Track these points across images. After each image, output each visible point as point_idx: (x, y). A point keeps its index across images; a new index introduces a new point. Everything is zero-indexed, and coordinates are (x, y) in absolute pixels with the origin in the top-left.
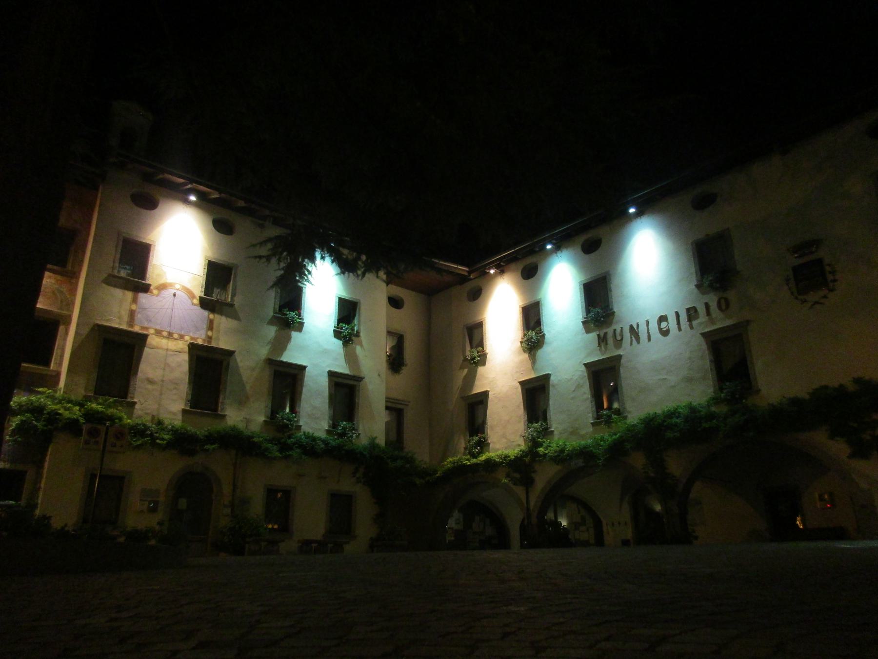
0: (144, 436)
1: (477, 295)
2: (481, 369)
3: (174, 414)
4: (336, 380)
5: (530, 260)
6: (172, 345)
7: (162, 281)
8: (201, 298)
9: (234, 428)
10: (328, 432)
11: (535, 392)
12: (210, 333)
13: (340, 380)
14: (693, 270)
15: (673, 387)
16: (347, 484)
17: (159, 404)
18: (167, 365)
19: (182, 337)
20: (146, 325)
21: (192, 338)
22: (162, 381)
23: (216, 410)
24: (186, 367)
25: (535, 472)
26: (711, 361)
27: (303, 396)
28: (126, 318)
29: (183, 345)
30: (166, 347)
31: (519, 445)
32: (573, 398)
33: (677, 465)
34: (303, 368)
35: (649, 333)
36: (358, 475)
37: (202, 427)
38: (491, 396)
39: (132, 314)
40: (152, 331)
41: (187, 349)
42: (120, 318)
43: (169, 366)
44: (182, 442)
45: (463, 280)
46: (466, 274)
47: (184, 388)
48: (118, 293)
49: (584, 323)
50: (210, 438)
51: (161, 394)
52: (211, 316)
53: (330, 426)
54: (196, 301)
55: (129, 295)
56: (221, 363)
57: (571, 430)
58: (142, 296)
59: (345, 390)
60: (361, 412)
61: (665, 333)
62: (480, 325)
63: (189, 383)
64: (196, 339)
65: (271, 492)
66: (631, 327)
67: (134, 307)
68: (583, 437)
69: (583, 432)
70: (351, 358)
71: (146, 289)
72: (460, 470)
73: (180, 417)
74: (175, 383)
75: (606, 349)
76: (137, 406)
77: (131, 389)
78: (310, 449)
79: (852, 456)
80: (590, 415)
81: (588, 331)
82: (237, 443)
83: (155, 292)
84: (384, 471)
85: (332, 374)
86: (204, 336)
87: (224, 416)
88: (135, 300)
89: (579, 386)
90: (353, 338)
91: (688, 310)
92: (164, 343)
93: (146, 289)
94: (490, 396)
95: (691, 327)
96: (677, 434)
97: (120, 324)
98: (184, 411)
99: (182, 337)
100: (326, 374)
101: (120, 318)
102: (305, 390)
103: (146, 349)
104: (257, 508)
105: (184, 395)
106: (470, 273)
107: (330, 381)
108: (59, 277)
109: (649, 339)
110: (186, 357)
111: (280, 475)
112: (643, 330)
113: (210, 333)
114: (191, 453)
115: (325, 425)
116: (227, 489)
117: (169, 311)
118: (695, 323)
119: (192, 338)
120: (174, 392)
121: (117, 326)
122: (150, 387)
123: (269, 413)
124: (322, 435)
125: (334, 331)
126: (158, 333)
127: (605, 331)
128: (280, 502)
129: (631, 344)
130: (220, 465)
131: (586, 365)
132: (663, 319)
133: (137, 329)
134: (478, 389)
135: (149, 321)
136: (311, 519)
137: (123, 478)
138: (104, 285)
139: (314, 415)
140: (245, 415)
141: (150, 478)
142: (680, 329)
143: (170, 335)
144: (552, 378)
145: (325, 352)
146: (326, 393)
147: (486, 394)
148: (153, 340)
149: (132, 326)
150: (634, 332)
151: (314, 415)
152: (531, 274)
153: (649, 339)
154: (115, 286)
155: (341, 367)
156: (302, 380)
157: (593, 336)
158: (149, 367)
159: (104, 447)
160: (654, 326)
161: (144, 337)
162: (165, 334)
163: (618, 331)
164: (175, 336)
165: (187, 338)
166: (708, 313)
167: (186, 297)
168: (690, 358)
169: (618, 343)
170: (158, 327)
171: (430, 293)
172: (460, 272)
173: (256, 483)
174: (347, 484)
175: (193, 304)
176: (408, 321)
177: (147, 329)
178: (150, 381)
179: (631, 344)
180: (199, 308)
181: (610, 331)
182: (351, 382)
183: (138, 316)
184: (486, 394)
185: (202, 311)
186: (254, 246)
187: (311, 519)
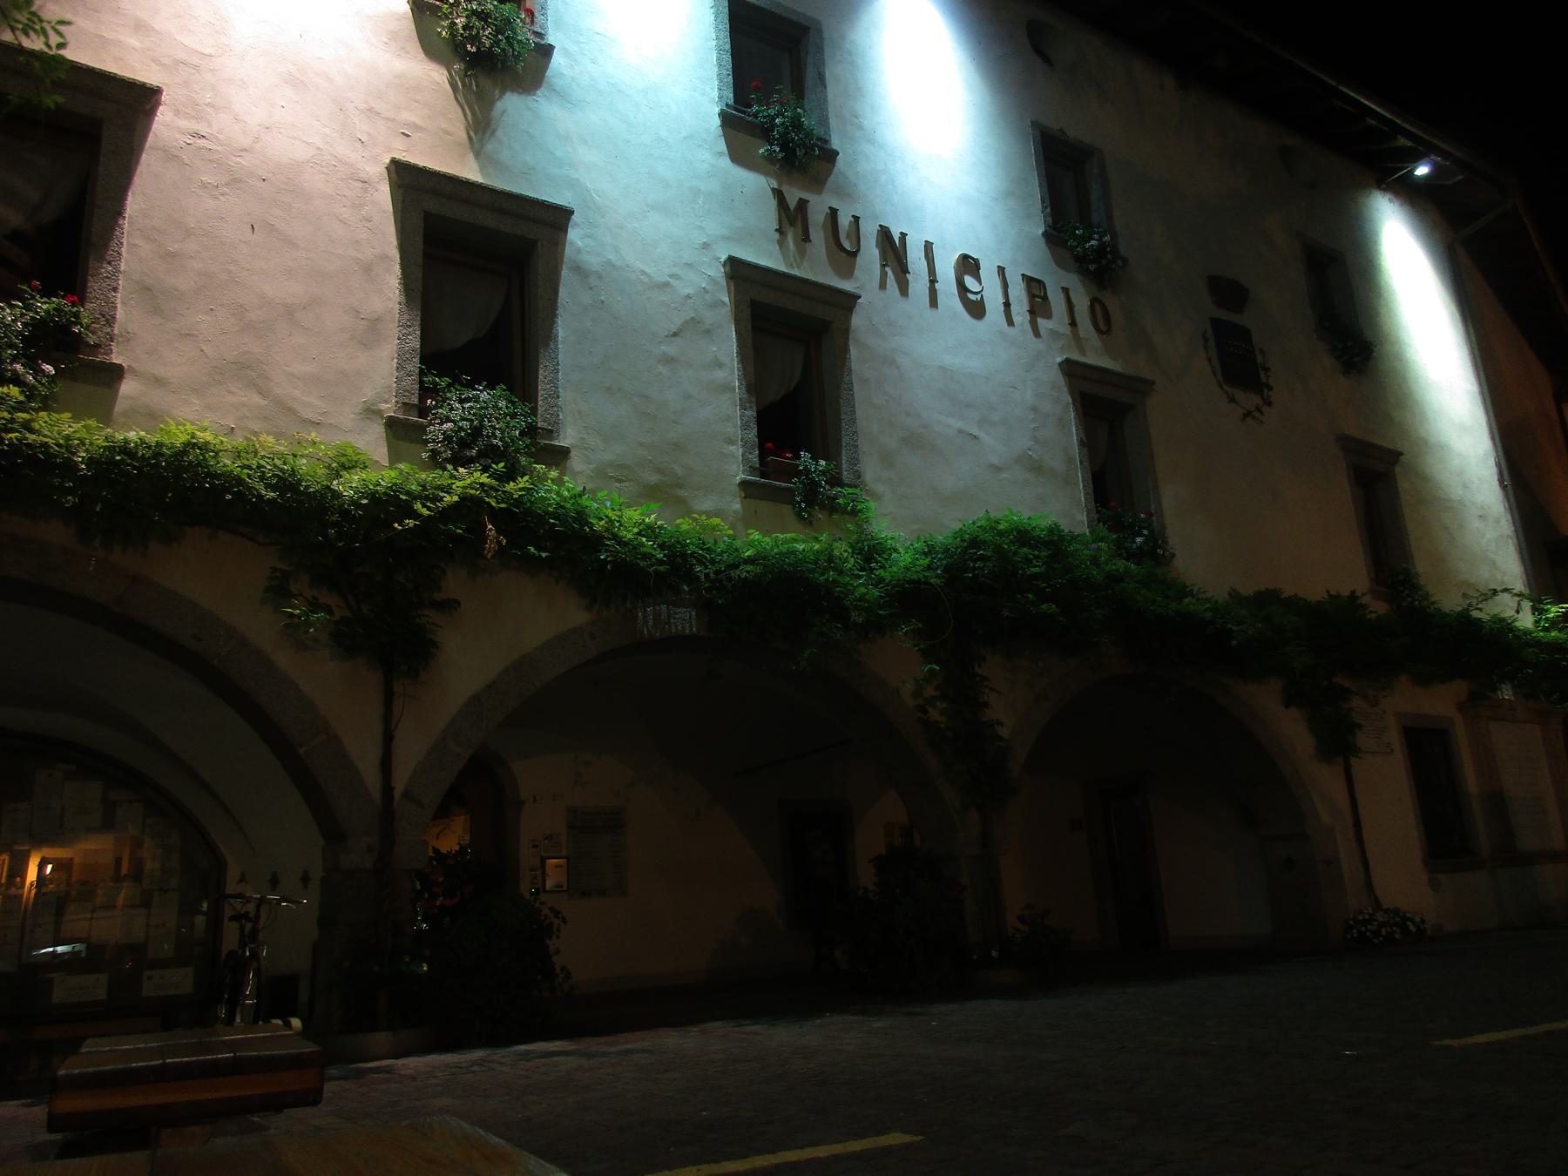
33: (1012, 701)
35: (933, 281)
38: (166, 124)
57: (654, 478)
61: (976, 309)
66: (885, 233)
75: (802, 253)
80: (737, 451)
89: (692, 327)
90: (31, 33)
96: (456, 498)
112: (915, 257)
127: (805, 196)
129: (883, 286)
132: (968, 265)
142: (1010, 322)
150: (893, 250)
153: (934, 303)
160: (946, 268)
163: (844, 221)
179: (883, 286)
186: (196, 67)
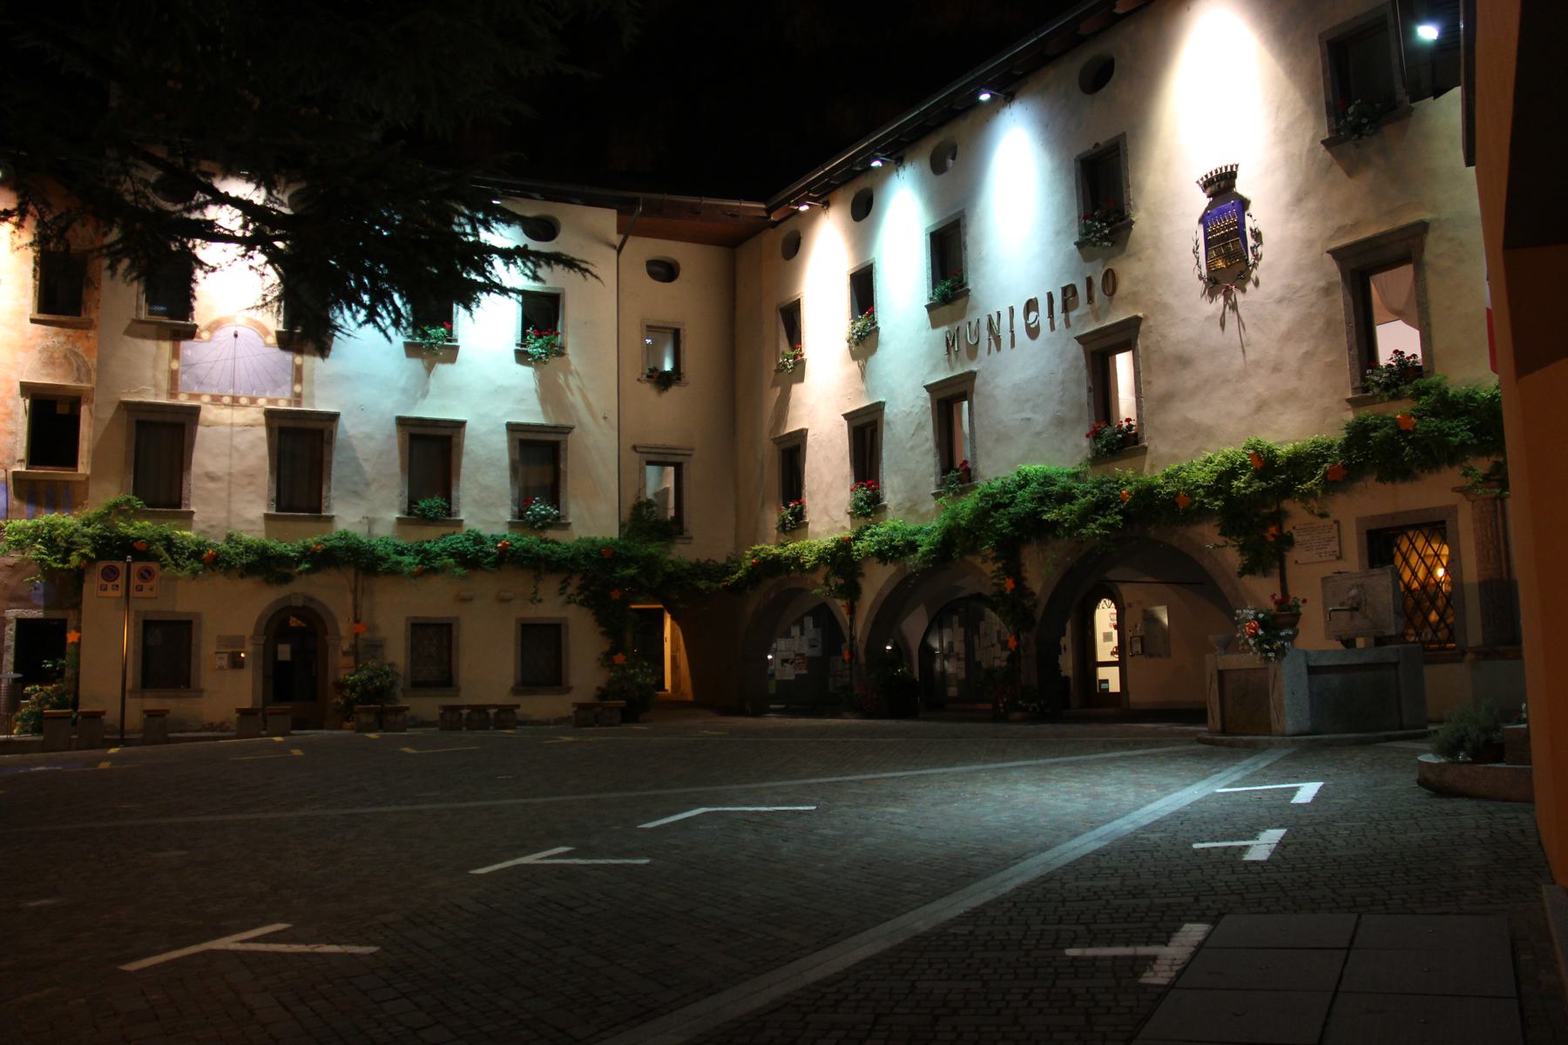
0: (211, 561)
1: (793, 247)
2: (797, 389)
3: (252, 522)
4: (523, 436)
5: (862, 184)
6: (239, 416)
7: (215, 316)
8: (278, 333)
9: (345, 536)
10: (511, 525)
11: (865, 430)
12: (298, 388)
13: (530, 436)
14: (1075, 214)
15: (1039, 434)
16: (551, 605)
17: (229, 511)
18: (232, 447)
19: (253, 401)
20: (196, 390)
21: (270, 401)
22: (230, 474)
23: (319, 510)
24: (263, 449)
25: (862, 575)
26: (1090, 390)
27: (463, 471)
28: (165, 384)
29: (255, 414)
30: (229, 421)
31: (844, 528)
32: (912, 448)
34: (460, 425)
36: (570, 590)
37: (300, 537)
39: (174, 376)
40: (206, 399)
41: (262, 419)
42: (156, 386)
43: (237, 450)
44: (263, 565)
45: (762, 226)
46: (764, 214)
47: (265, 480)
48: (150, 346)
49: (930, 308)
50: (307, 554)
51: (230, 495)
52: (298, 360)
53: (514, 516)
54: (272, 339)
55: (167, 346)
56: (321, 432)
58: (186, 346)
59: (539, 453)
60: (573, 486)
62: (796, 306)
63: (271, 473)
64: (274, 401)
65: (419, 629)
67: (175, 365)
68: (923, 517)
69: (923, 510)
70: (549, 393)
71: (191, 333)
72: (774, 566)
73: (261, 525)
74: (251, 475)
76: (195, 518)
77: (185, 492)
78: (476, 558)
79: (1247, 570)
81: (935, 324)
82: (357, 560)
83: (205, 335)
84: (631, 580)
85: (512, 428)
86: (288, 395)
87: (330, 519)
88: (176, 354)
91: (1065, 290)
92: (225, 415)
93: (191, 333)
94: (810, 439)
95: (1068, 324)
97: (156, 395)
98: (267, 517)
99: (253, 401)
100: (504, 429)
101: (156, 386)
102: (465, 461)
103: (200, 429)
104: (397, 654)
105: (265, 492)
106: (769, 211)
107: (511, 441)
108: (70, 331)
109: (1013, 345)
110: (262, 432)
111: (432, 600)
113: (298, 388)
114: (286, 579)
115: (506, 514)
116: (345, 627)
117: (229, 363)
118: (1073, 314)
119: (270, 401)
120: (252, 488)
121: (152, 400)
122: (211, 485)
123: (406, 506)
124: (500, 530)
125: (517, 352)
126: (216, 400)
128: (435, 641)
130: (330, 593)
131: (928, 388)
133: (183, 400)
134: (792, 427)
135: (201, 383)
136: (488, 668)
137: (190, 622)
138: (128, 338)
139: (485, 502)
140: (367, 508)
141: (231, 616)
142: (1053, 328)
143: (235, 401)
144: (886, 410)
145: (500, 391)
146: (505, 460)
147: (802, 435)
148: (209, 413)
149: (173, 392)
151: (485, 502)
152: (863, 209)
153: (1013, 345)
154: (144, 337)
155: (532, 414)
156: (460, 445)
157: (941, 332)
158: (207, 456)
159: (128, 595)
161: (194, 412)
162: (227, 400)
164: (244, 401)
165: (262, 401)
166: (1090, 299)
167: (255, 335)
168: (1063, 382)
169: (972, 351)
170: (215, 392)
171: (733, 243)
172: (753, 214)
173: (392, 614)
174: (551, 605)
175: (267, 345)
176: (683, 302)
177: (197, 396)
178: (212, 477)
180: (277, 350)
181: (962, 324)
182: (552, 437)
183: (183, 378)
184: (802, 435)
185: (282, 353)
187: (488, 668)
